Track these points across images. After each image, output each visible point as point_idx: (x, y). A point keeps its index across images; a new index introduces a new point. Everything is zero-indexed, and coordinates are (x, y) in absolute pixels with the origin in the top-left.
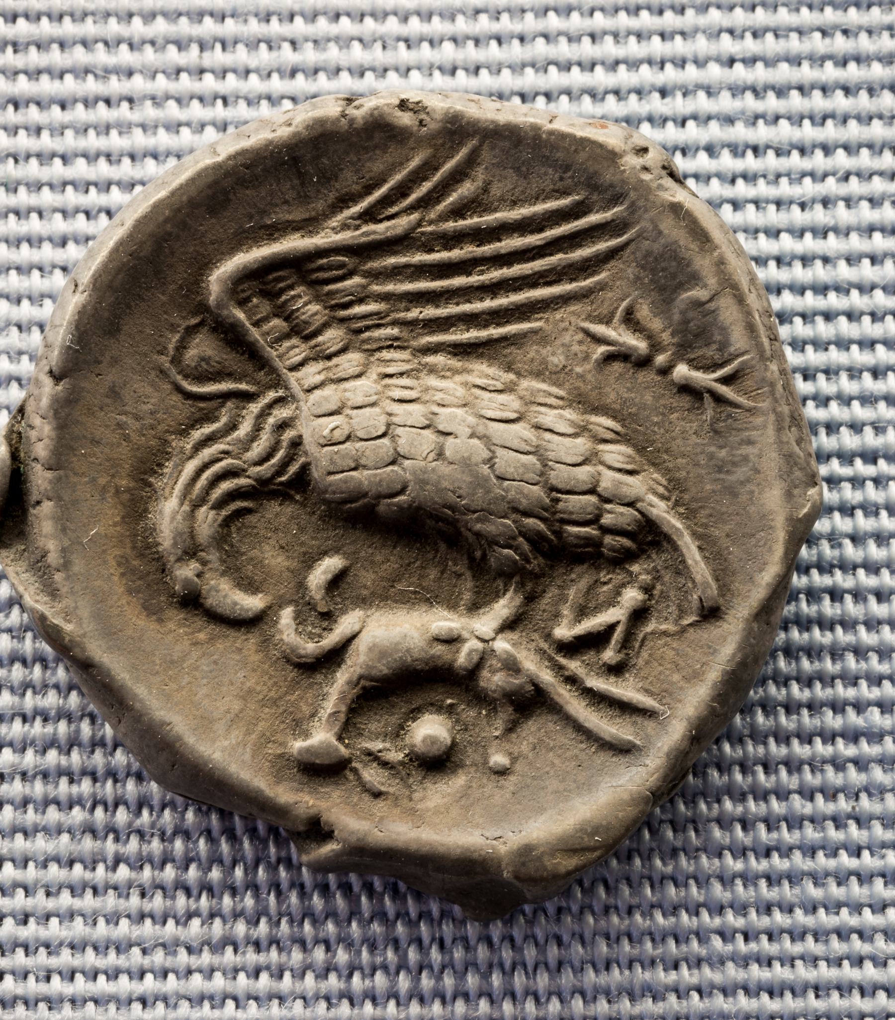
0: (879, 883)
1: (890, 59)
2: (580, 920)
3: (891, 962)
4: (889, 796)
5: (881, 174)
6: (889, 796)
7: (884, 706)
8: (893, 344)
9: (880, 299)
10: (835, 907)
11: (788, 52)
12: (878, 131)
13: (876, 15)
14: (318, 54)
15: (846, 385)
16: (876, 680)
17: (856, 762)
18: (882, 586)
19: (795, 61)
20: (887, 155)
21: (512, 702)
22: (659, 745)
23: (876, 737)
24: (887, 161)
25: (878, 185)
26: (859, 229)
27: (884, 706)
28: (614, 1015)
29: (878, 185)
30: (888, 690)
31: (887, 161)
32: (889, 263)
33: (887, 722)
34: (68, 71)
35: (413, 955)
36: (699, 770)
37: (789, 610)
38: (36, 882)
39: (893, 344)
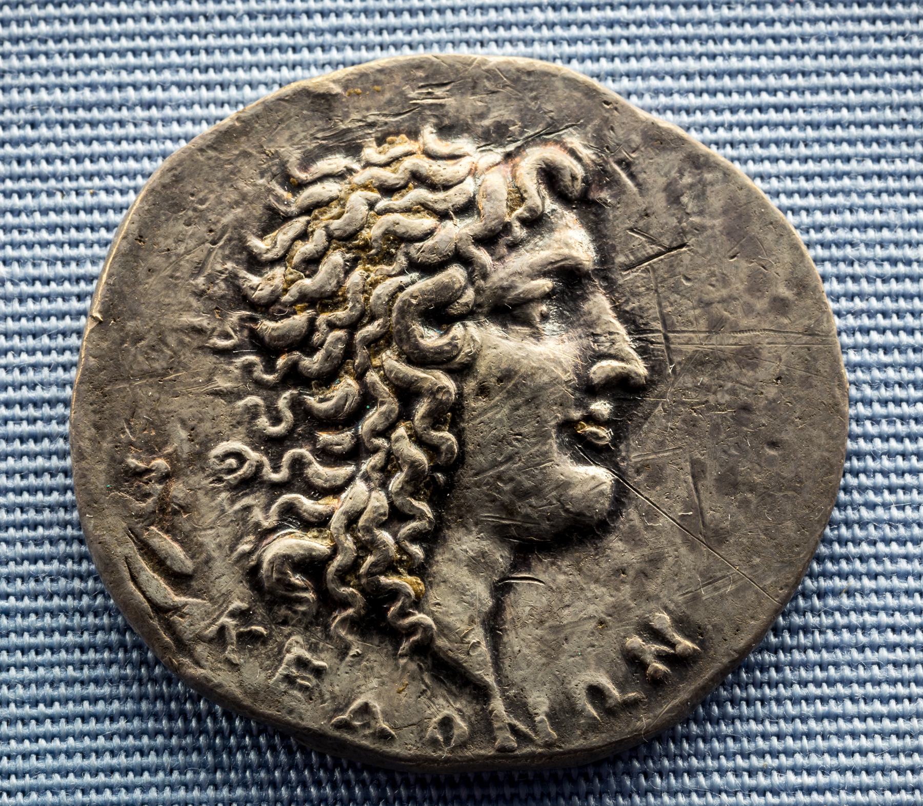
0: (914, 459)
1: (919, 611)
2: (533, 374)
5: (914, 157)
7: (916, 385)
9: (913, 654)
13: (915, 9)
14: (584, 693)
15: (890, 601)
16: (911, 332)
18: (912, 729)
19: (875, 125)
21: (575, 310)
23: (910, 402)
32: (919, 667)
33: (919, 394)
35: (209, 723)
36: (706, 705)
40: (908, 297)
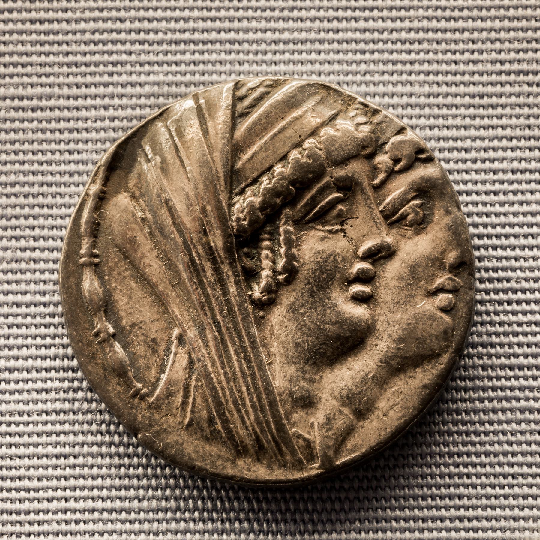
3: (538, 498)
4: (538, 335)
6: (538, 335)
8: (539, 225)
10: (504, 248)
11: (497, 135)
12: (533, 165)
17: (510, 410)
20: (537, 174)
22: (337, 374)
23: (532, 312)
24: (537, 176)
25: (533, 186)
26: (519, 247)
27: (536, 302)
28: (350, 175)
29: (533, 186)
30: (537, 295)
31: (537, 176)
33: (537, 329)
34: (18, 205)
37: (457, 374)
38: (21, 8)
39: (539, 225)
40: (532, 291)
